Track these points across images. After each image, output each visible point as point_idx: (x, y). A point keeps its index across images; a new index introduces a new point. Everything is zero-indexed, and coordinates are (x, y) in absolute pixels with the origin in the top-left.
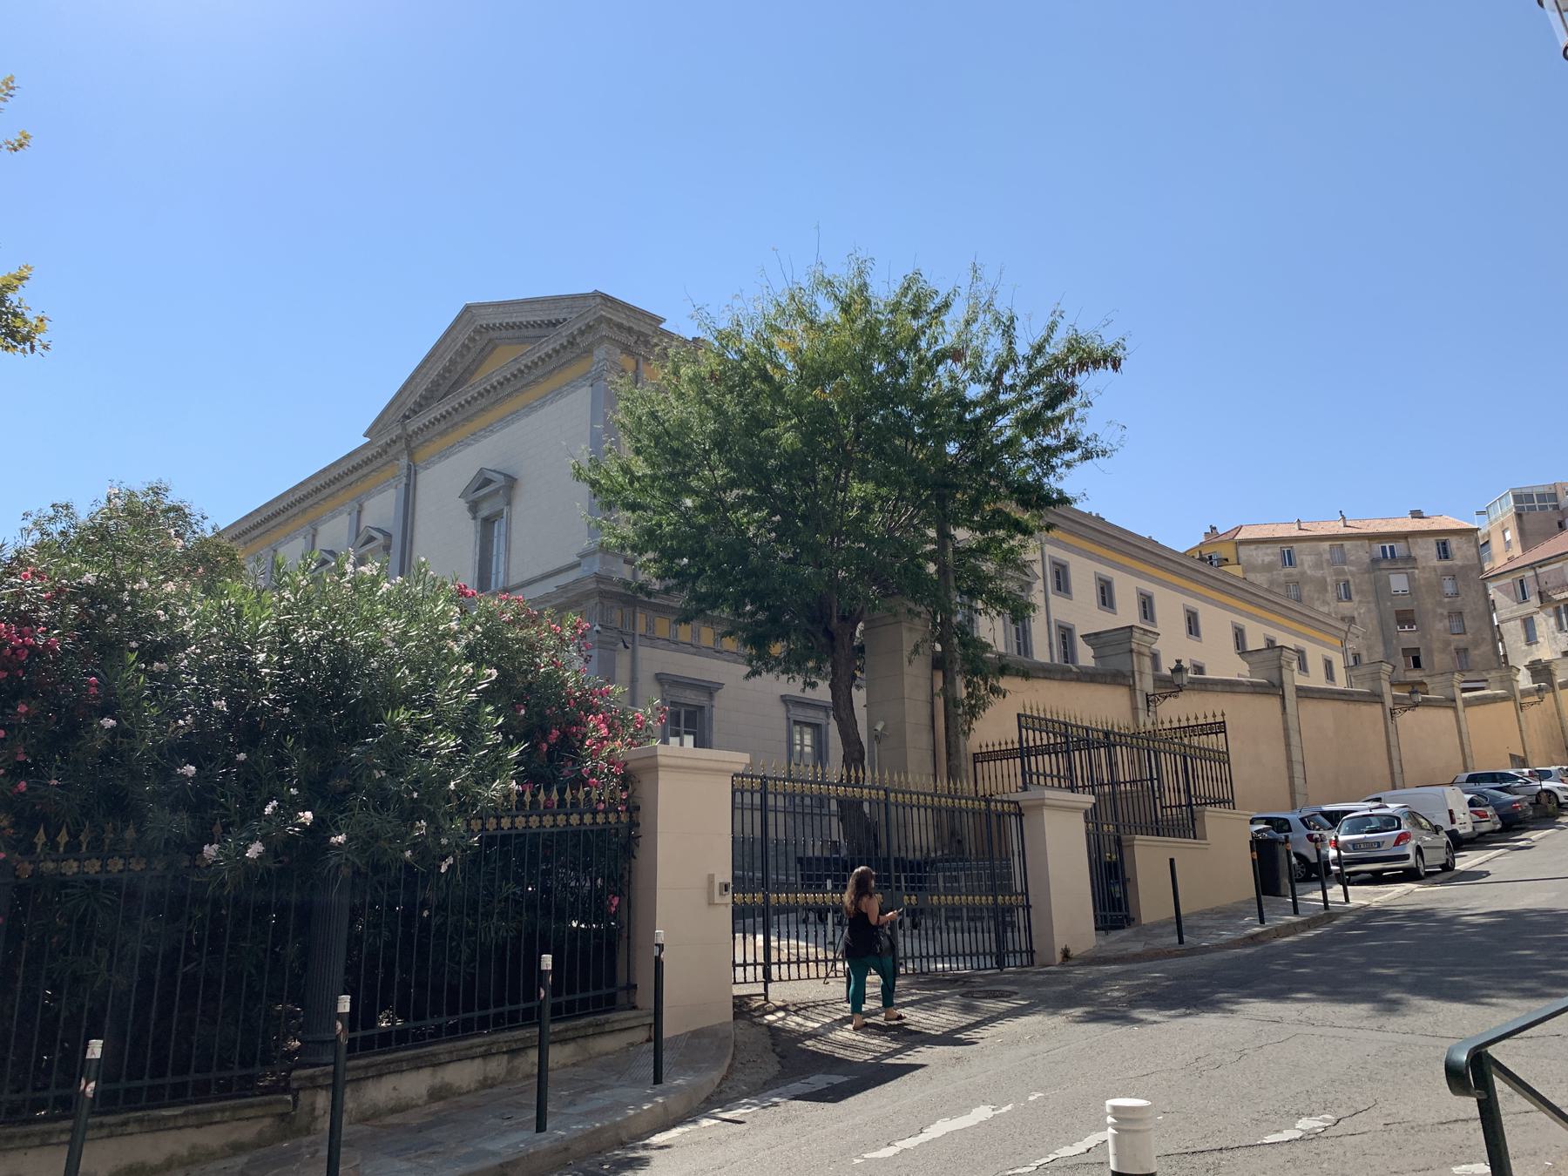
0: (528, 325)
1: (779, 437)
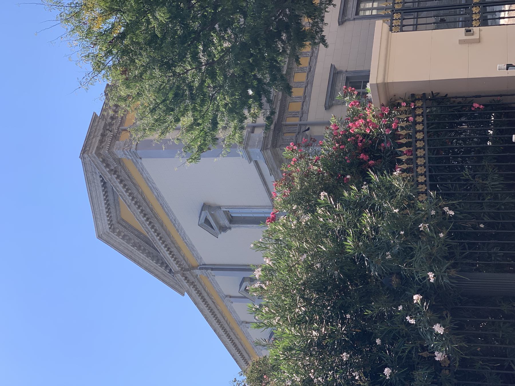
0: (107, 200)
1: (161, 24)
